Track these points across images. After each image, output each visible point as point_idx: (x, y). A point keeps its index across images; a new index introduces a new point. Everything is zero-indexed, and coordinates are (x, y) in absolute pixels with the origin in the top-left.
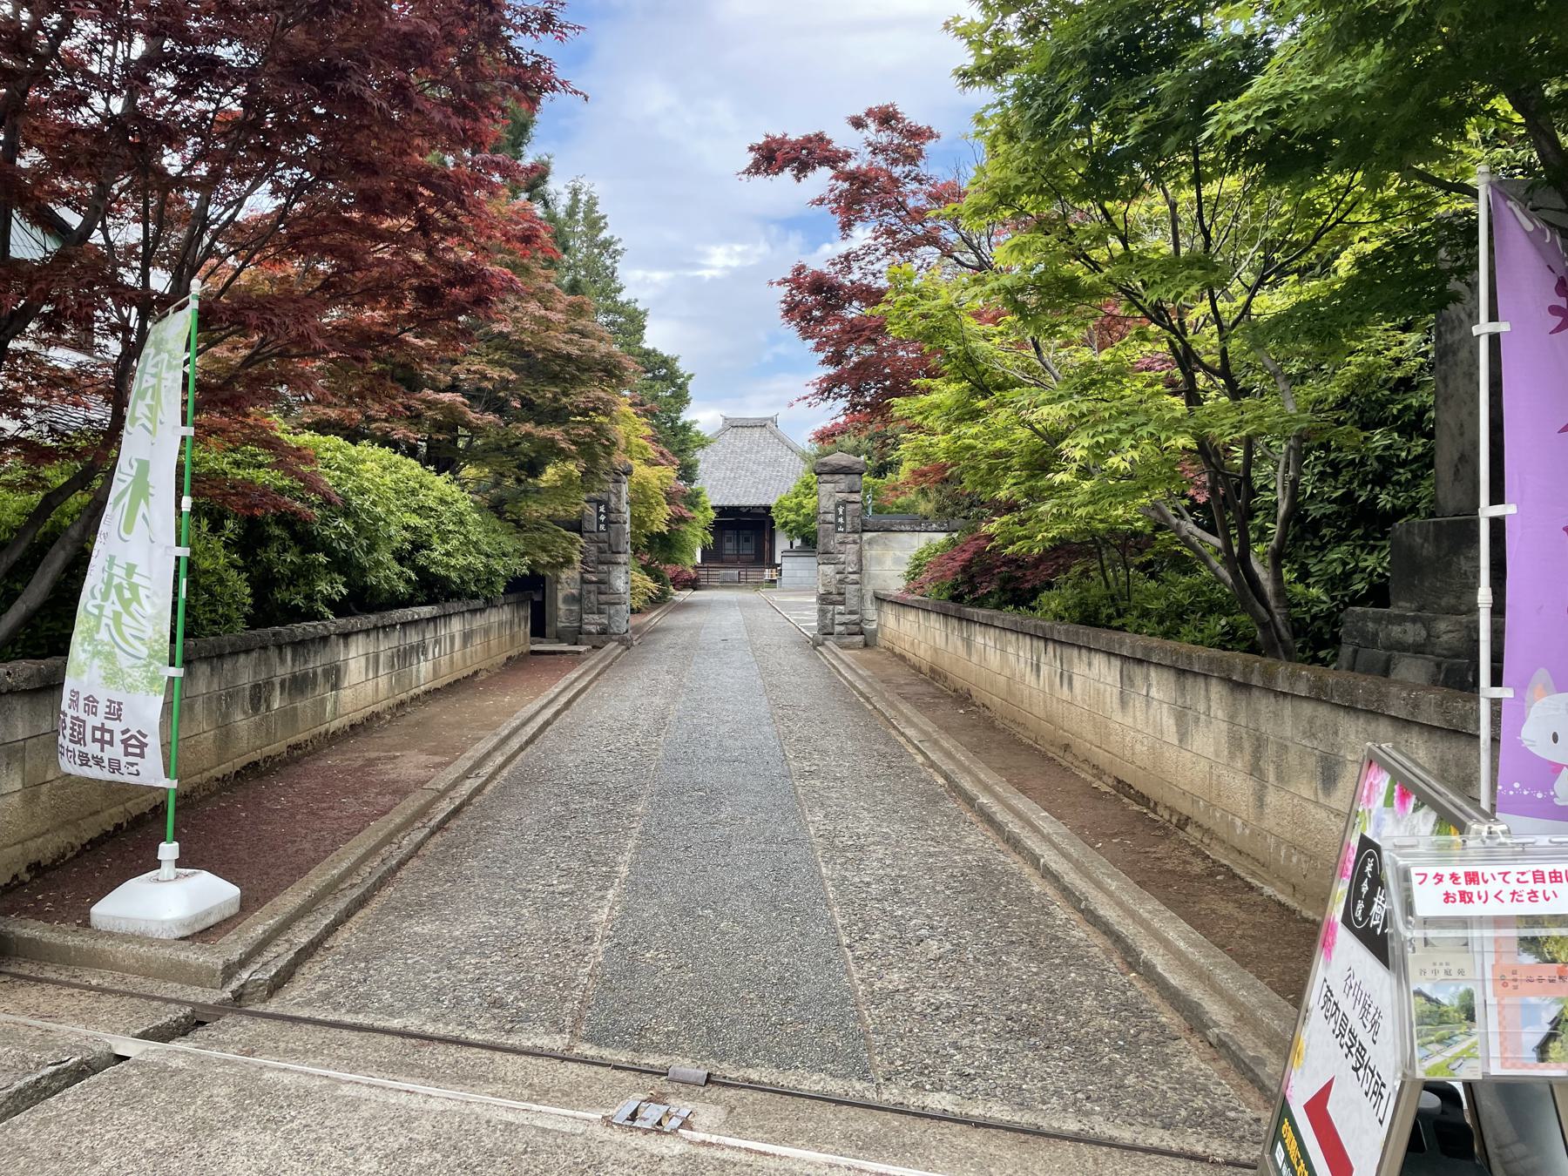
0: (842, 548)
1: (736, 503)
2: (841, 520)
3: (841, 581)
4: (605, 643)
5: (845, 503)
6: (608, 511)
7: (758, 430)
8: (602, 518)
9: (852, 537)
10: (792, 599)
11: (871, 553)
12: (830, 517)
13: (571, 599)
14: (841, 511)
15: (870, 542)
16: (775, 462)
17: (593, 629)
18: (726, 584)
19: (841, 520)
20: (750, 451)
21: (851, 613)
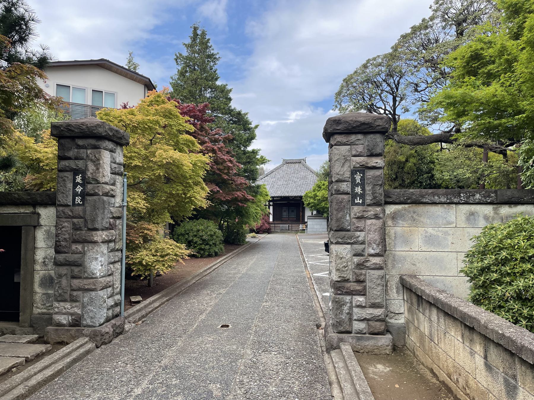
0: (361, 224)
1: (287, 195)
2: (358, 190)
3: (360, 266)
4: (74, 338)
5: (364, 168)
6: (85, 182)
7: (297, 165)
8: (79, 189)
9: (372, 211)
10: (311, 241)
11: (396, 230)
12: (345, 187)
13: (48, 282)
14: (358, 178)
15: (394, 217)
16: (305, 177)
17: (64, 319)
18: (283, 231)
19: (358, 190)
20: (294, 173)
21: (374, 306)
